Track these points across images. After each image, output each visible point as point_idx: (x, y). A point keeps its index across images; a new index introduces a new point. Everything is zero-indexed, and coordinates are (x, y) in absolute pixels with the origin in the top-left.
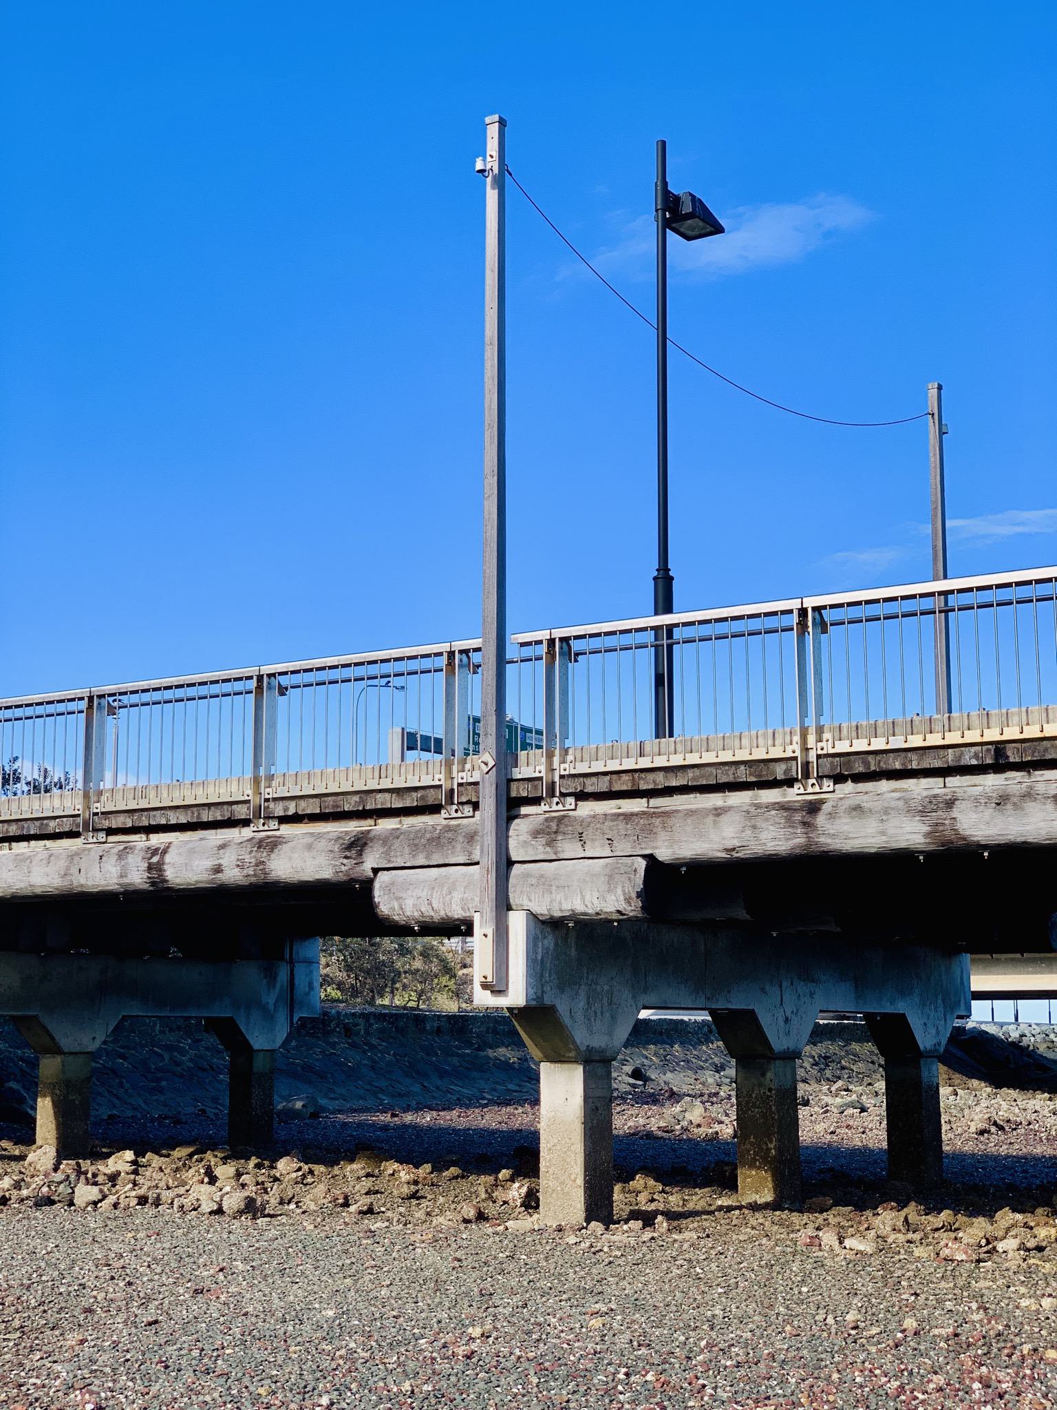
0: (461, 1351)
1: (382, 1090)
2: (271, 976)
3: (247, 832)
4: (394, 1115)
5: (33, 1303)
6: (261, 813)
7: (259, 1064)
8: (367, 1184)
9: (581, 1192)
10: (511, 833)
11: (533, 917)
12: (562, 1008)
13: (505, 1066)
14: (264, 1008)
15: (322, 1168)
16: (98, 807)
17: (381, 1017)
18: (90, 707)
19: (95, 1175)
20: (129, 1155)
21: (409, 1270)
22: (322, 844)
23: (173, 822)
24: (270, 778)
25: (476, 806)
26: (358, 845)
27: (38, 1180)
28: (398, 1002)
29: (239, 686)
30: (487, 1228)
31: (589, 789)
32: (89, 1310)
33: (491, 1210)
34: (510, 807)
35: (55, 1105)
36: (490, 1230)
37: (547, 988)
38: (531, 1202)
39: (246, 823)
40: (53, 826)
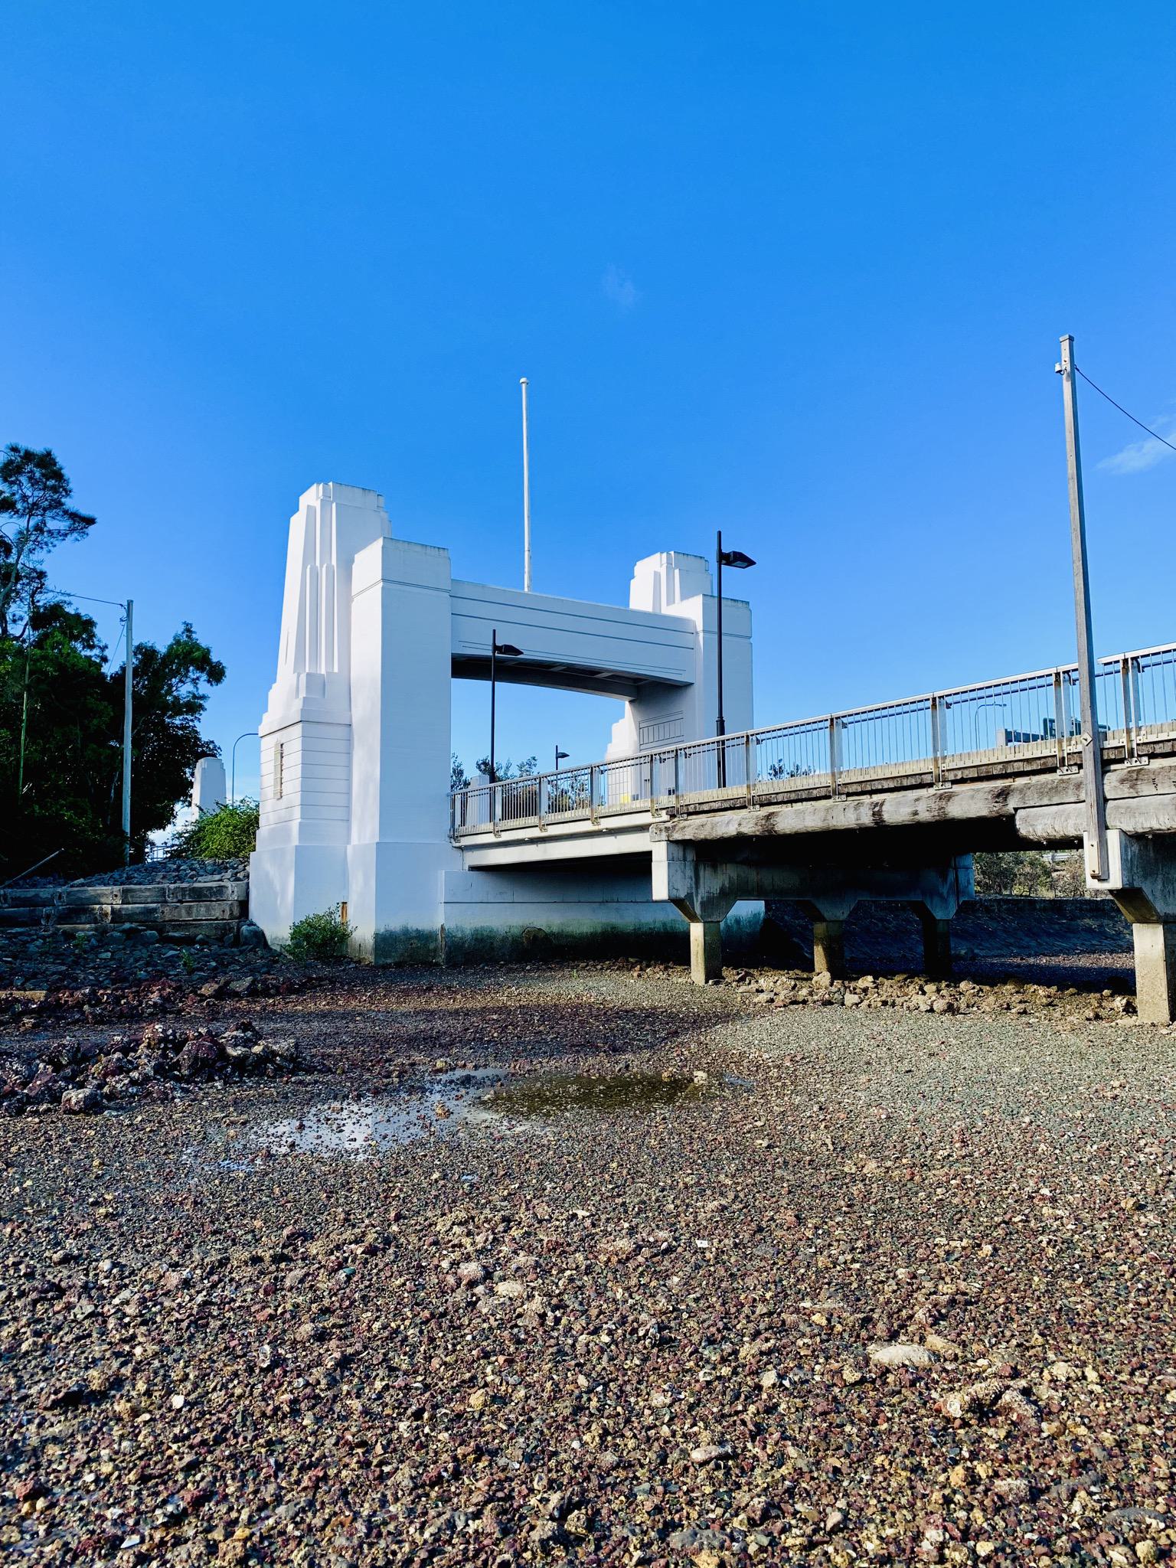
0: (1109, 1094)
1: (1011, 945)
2: (945, 878)
3: (932, 791)
4: (1022, 959)
5: (835, 1058)
6: (941, 779)
7: (941, 927)
8: (1018, 997)
9: (1166, 1003)
10: (1105, 781)
11: (1123, 832)
12: (1147, 889)
13: (1089, 930)
14: (941, 896)
15: (988, 988)
16: (840, 781)
17: (1007, 901)
18: (832, 724)
19: (854, 989)
20: (870, 978)
21: (1060, 1046)
22: (981, 795)
23: (886, 787)
24: (944, 758)
25: (1080, 766)
26: (1003, 794)
27: (822, 992)
28: (1015, 892)
29: (921, 705)
30: (1104, 1024)
31: (1158, 751)
32: (868, 1063)
33: (1102, 1013)
34: (1104, 765)
35: (824, 949)
36: (1107, 1025)
37: (1136, 877)
38: (1130, 1009)
39: (931, 785)
40: (815, 793)
